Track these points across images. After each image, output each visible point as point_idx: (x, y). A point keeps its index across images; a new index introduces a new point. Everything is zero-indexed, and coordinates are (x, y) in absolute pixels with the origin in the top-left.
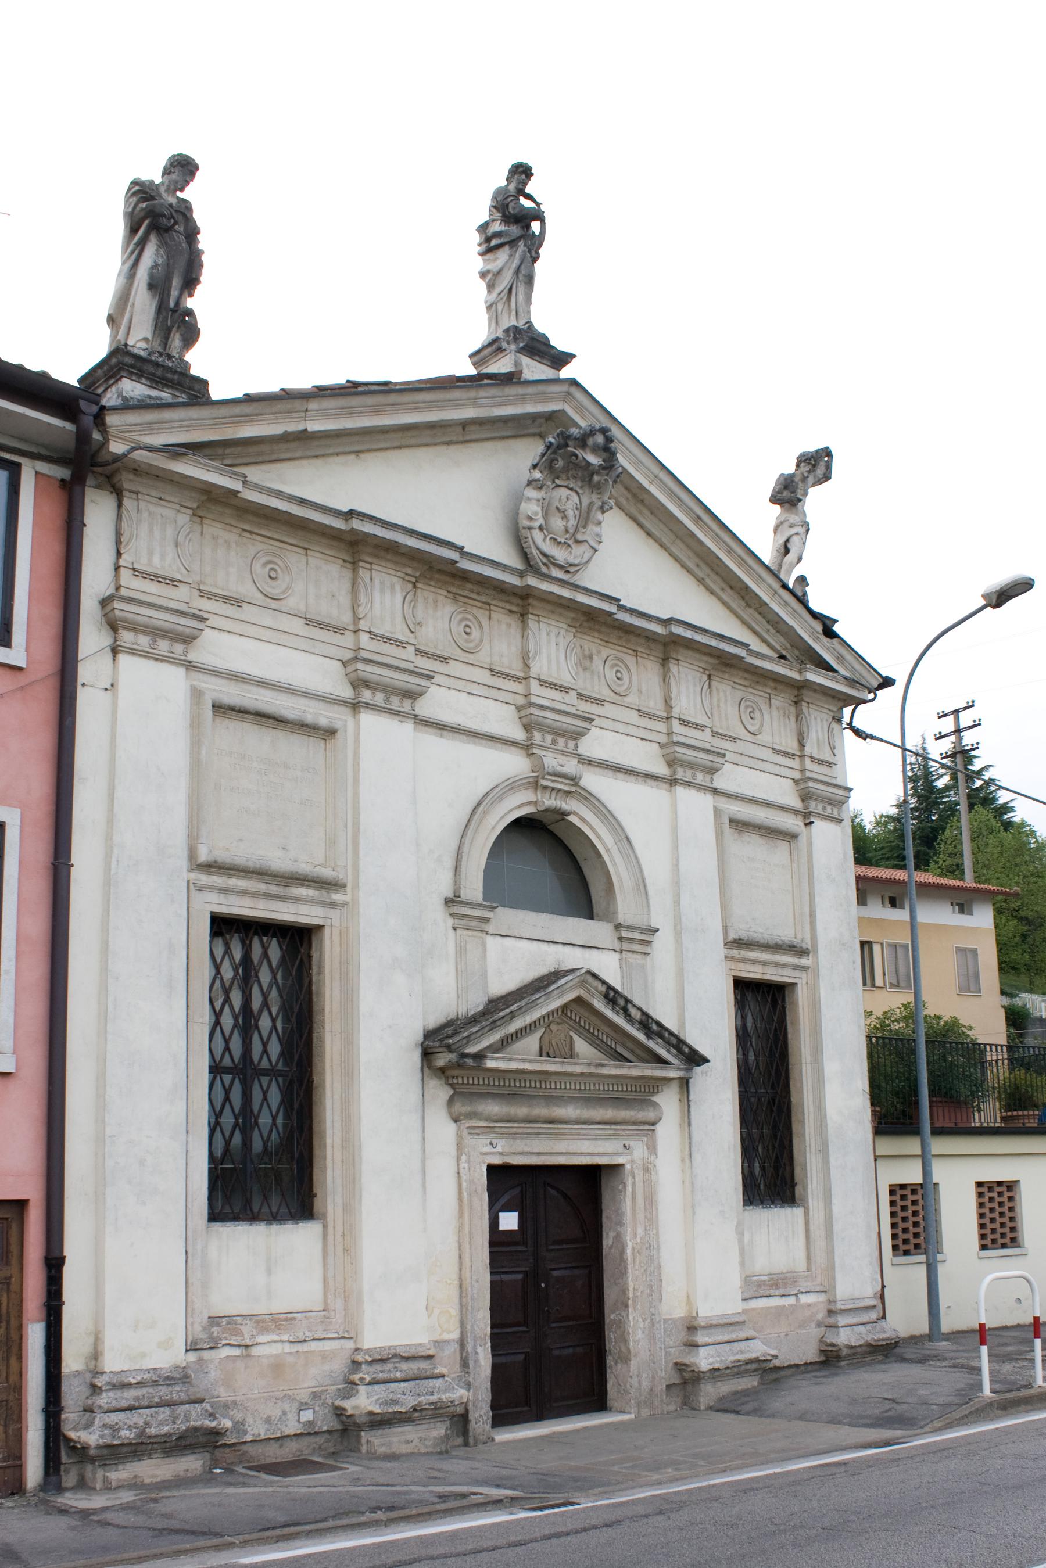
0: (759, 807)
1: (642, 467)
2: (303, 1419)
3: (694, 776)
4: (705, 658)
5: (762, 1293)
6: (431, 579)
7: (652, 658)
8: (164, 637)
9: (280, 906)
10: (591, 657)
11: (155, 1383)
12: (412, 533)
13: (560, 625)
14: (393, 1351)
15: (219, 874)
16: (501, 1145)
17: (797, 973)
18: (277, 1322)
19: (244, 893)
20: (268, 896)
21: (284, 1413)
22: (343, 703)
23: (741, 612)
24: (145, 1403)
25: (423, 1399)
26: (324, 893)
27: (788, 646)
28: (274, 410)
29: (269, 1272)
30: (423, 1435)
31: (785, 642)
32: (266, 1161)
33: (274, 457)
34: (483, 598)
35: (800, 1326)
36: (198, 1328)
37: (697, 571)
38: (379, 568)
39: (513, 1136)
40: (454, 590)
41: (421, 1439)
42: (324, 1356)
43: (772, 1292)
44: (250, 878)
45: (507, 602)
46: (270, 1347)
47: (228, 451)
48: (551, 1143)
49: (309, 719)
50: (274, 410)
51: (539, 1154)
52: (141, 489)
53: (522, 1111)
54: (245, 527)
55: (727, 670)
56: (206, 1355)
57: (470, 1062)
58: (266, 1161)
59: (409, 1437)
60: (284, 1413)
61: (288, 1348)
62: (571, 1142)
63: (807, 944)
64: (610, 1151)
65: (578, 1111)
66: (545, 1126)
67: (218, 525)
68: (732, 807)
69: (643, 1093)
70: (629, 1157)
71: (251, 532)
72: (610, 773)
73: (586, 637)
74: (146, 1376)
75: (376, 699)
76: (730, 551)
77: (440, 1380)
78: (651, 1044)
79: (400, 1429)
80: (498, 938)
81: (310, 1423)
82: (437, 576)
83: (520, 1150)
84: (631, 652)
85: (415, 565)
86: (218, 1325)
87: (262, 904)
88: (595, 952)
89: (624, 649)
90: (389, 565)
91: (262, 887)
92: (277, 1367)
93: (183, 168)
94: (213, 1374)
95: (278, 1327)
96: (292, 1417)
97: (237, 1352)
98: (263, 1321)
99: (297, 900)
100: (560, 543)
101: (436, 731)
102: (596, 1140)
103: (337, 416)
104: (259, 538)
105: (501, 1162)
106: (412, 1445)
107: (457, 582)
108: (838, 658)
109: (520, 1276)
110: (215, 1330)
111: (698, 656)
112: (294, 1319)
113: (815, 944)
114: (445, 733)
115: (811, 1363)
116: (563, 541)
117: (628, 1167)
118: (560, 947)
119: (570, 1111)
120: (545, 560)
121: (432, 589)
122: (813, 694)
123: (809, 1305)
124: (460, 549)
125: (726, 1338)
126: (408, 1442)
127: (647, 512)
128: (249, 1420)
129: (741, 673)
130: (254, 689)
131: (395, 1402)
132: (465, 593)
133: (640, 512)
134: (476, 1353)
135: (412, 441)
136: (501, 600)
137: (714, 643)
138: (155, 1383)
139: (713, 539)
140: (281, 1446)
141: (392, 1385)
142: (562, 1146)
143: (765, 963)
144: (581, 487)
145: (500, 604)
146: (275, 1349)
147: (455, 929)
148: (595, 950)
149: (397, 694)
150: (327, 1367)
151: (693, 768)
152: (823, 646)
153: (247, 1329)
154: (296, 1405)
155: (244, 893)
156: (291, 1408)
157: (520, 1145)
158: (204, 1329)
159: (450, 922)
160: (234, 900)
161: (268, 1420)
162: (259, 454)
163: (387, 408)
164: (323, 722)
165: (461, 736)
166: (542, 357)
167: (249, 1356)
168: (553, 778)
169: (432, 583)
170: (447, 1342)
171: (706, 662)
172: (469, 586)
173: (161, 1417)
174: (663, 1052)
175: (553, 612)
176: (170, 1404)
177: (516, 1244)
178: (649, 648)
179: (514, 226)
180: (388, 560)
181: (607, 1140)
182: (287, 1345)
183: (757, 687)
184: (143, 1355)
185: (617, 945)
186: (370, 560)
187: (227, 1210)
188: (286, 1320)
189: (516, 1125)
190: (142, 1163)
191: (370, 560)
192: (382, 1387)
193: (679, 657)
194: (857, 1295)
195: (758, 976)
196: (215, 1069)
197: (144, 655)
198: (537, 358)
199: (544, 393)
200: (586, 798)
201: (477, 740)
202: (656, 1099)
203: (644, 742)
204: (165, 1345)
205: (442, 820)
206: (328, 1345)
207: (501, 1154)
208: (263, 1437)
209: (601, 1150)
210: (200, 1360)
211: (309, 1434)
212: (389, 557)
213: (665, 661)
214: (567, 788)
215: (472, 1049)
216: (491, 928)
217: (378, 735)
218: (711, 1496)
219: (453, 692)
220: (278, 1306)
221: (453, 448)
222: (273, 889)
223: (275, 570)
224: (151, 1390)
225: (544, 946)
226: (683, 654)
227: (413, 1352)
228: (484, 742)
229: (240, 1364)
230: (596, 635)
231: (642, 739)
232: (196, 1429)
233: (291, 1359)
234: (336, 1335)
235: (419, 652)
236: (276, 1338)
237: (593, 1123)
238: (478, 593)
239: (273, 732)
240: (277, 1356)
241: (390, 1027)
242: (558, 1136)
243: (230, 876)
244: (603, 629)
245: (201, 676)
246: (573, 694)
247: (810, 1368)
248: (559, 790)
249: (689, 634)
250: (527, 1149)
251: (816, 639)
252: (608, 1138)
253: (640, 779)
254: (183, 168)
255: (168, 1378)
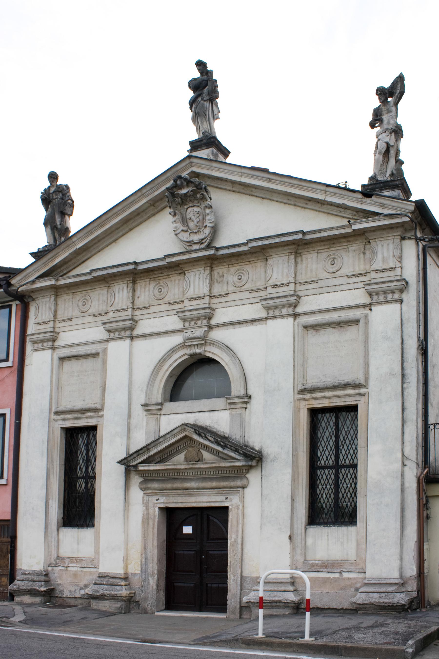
0: (355, 310)
1: (234, 173)
2: (81, 593)
3: (281, 312)
4: (286, 248)
5: (313, 569)
6: (141, 277)
7: (260, 261)
8: (45, 342)
9: (80, 421)
10: (223, 276)
11: (34, 574)
12: (113, 267)
13: (200, 269)
14: (107, 574)
15: (63, 415)
16: (162, 500)
17: (357, 398)
18: (77, 560)
19: (69, 419)
20: (77, 418)
21: (76, 590)
22: (363, 306)
23: (321, 210)
24: (27, 579)
25: (105, 592)
26: (97, 413)
27: (355, 213)
28: (62, 249)
29: (78, 544)
30: (111, 605)
31: (352, 212)
32: (78, 509)
33: (80, 262)
34: (165, 274)
35: (341, 589)
36: (52, 560)
37: (289, 202)
38: (117, 284)
39: (167, 495)
40: (152, 277)
41: (110, 606)
42: (91, 573)
43: (321, 570)
44: (71, 414)
45: (175, 271)
46: (74, 568)
47: (62, 269)
48: (187, 498)
49: (89, 352)
50: (62, 249)
51: (182, 503)
52: (38, 296)
53: (169, 485)
54: (74, 291)
55: (308, 246)
56: (54, 568)
57: (132, 468)
58: (78, 509)
59: (106, 605)
60: (76, 590)
61: (79, 569)
62: (198, 497)
63: (363, 382)
64: (218, 500)
65: (197, 484)
66: (182, 491)
67: (65, 295)
68: (312, 319)
69: (239, 473)
70: (231, 503)
71: (76, 292)
72: (231, 327)
73: (219, 268)
74: (31, 572)
75: (275, 313)
76: (292, 185)
77: (120, 587)
78: (225, 451)
79: (104, 602)
80: (167, 416)
81: (83, 595)
82: (142, 275)
83: (172, 501)
84: (248, 263)
85: (128, 276)
86: (59, 559)
87: (76, 421)
88: (216, 412)
89: (243, 264)
90: (120, 281)
91: (76, 416)
92: (75, 575)
93: (53, 177)
94: (56, 574)
95: (77, 562)
96: (78, 591)
97: (63, 568)
98: (73, 560)
99: (86, 418)
100: (196, 233)
101: (143, 338)
102: (210, 496)
103: (87, 236)
104: (79, 293)
105: (164, 506)
106: (107, 608)
107: (151, 273)
108: (381, 206)
109: (193, 552)
110: (58, 561)
111: (281, 249)
112: (82, 560)
113: (367, 379)
114: (148, 338)
115: (346, 609)
116: (196, 231)
117: (230, 507)
118: (197, 414)
119: (193, 484)
120: (188, 244)
121: (143, 281)
122: (375, 233)
123: (349, 579)
124: (135, 263)
125: (270, 589)
126: (105, 606)
127: (254, 190)
128: (65, 590)
129: (318, 244)
130: (76, 348)
131: (98, 592)
132: (157, 275)
133: (252, 191)
134: (149, 580)
135: (134, 225)
136: (173, 271)
137: (277, 240)
138: (34, 574)
139: (282, 184)
140: (76, 601)
141: (102, 586)
142: (193, 499)
143: (330, 397)
144: (199, 203)
145: (173, 273)
146: (75, 569)
147: (146, 415)
148: (217, 411)
149: (122, 331)
150: (91, 577)
151: (278, 308)
152: (369, 204)
153: (67, 562)
154: (79, 588)
155: (69, 419)
156: (78, 589)
157: (172, 499)
158: (54, 560)
159: (145, 413)
160: (67, 422)
161: (70, 591)
162: (75, 263)
163: (105, 222)
164: (94, 352)
165: (155, 337)
166: (201, 147)
167: (67, 570)
168: (191, 341)
169: (143, 278)
170: (137, 574)
171: (288, 249)
172: (156, 272)
173: (29, 584)
174: (232, 454)
175: (194, 266)
176: (34, 581)
177: (192, 539)
178: (255, 257)
179: (204, 90)
180: (118, 279)
181: (217, 495)
182: (79, 568)
183: (336, 245)
184: (32, 566)
185: (228, 407)
186: (112, 282)
187: (78, 523)
188: (80, 560)
189: (167, 491)
190: (33, 509)
191: (112, 282)
192: (98, 586)
193: (271, 254)
194: (384, 576)
195: (326, 405)
196: (94, 477)
197: (382, 303)
198: (199, 149)
199: (178, 171)
200: (213, 344)
201: (162, 335)
202: (247, 476)
203: (254, 305)
204: (38, 563)
205: (143, 373)
206: (92, 570)
207: (164, 503)
208: (69, 596)
209: (214, 500)
210: (53, 569)
211: (83, 598)
212: (117, 278)
213: (57, 296)
214: (199, 343)
215: (134, 464)
216: (163, 412)
217: (118, 350)
218: (42, 638)
219: (152, 319)
220: (80, 555)
221: (157, 216)
222: (79, 415)
223: (241, 276)
224: (32, 576)
225: (189, 415)
226: (271, 252)
227: (115, 575)
228: (165, 335)
229: (64, 572)
230: (225, 264)
231: (252, 304)
232: (35, 589)
233: (80, 573)
234: (93, 567)
235: (274, 286)
236: (75, 565)
237: (179, 489)
238: (161, 273)
239: (82, 361)
240: (76, 571)
241: (113, 458)
242: (190, 495)
243: (66, 414)
244: (226, 260)
245: (60, 350)
246: (186, 302)
247: (348, 612)
248: (197, 345)
249: (260, 243)
250: (175, 501)
251: (362, 203)
252: (217, 494)
253: (249, 324)
254: (53, 177)
255: (37, 573)
